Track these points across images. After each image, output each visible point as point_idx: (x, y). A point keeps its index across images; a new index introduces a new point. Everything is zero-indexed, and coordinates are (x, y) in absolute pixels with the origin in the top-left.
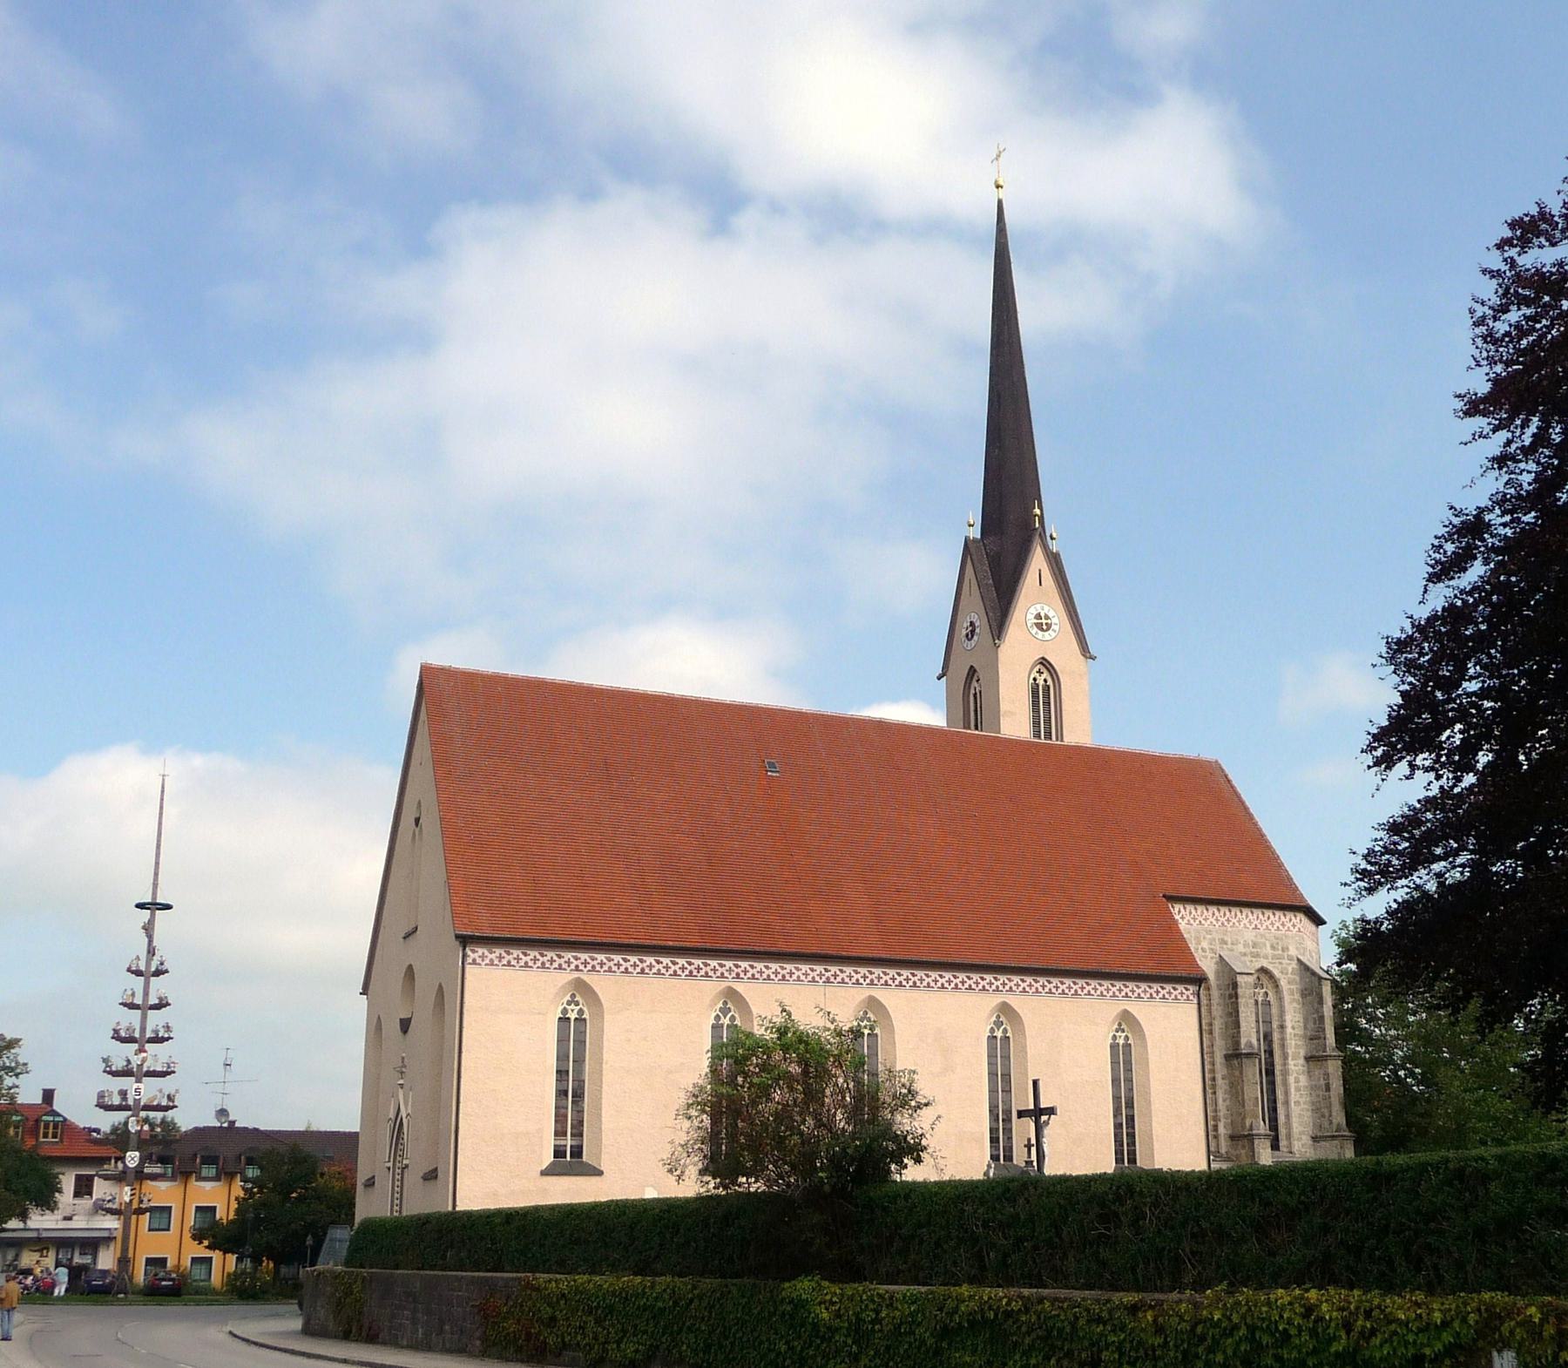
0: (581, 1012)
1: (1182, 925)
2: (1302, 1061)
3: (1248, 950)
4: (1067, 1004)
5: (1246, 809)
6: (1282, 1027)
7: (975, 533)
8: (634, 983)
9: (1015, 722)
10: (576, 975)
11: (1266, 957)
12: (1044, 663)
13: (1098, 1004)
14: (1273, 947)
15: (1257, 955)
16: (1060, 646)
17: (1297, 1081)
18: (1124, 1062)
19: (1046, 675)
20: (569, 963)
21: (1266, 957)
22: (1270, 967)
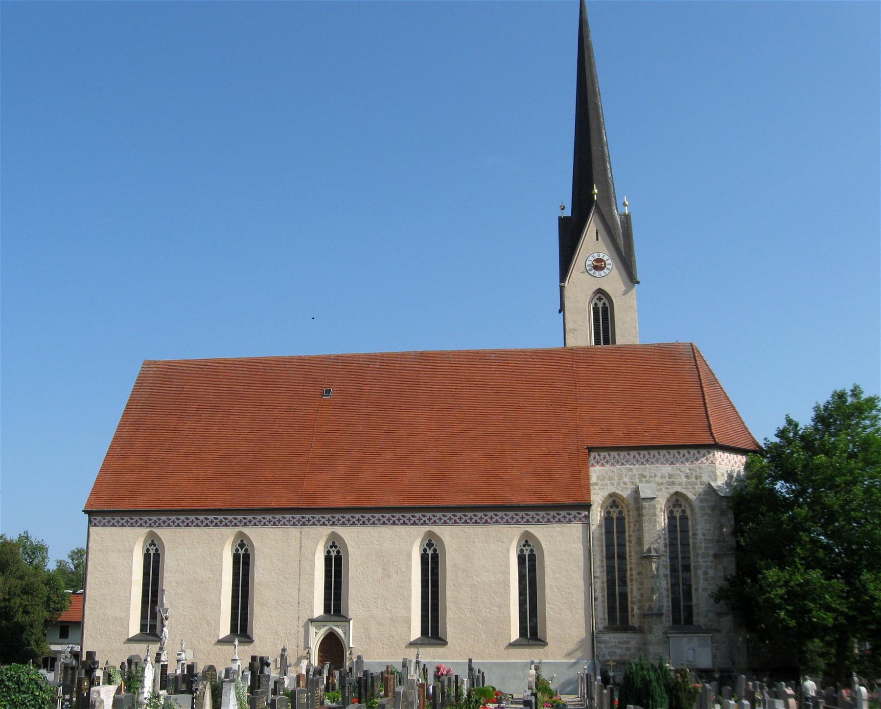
0: (684, 511)
1: (740, 457)
2: (710, 559)
3: (664, 481)
4: (480, 530)
5: (128, 406)
6: (694, 534)
7: (568, 213)
8: (183, 532)
9: (582, 335)
10: (149, 529)
11: (680, 484)
12: (600, 292)
13: (504, 529)
14: (687, 477)
15: (673, 483)
16: (612, 280)
17: (705, 573)
18: (530, 565)
19: (605, 300)
20: (146, 522)
21: (680, 484)
22: (684, 491)
